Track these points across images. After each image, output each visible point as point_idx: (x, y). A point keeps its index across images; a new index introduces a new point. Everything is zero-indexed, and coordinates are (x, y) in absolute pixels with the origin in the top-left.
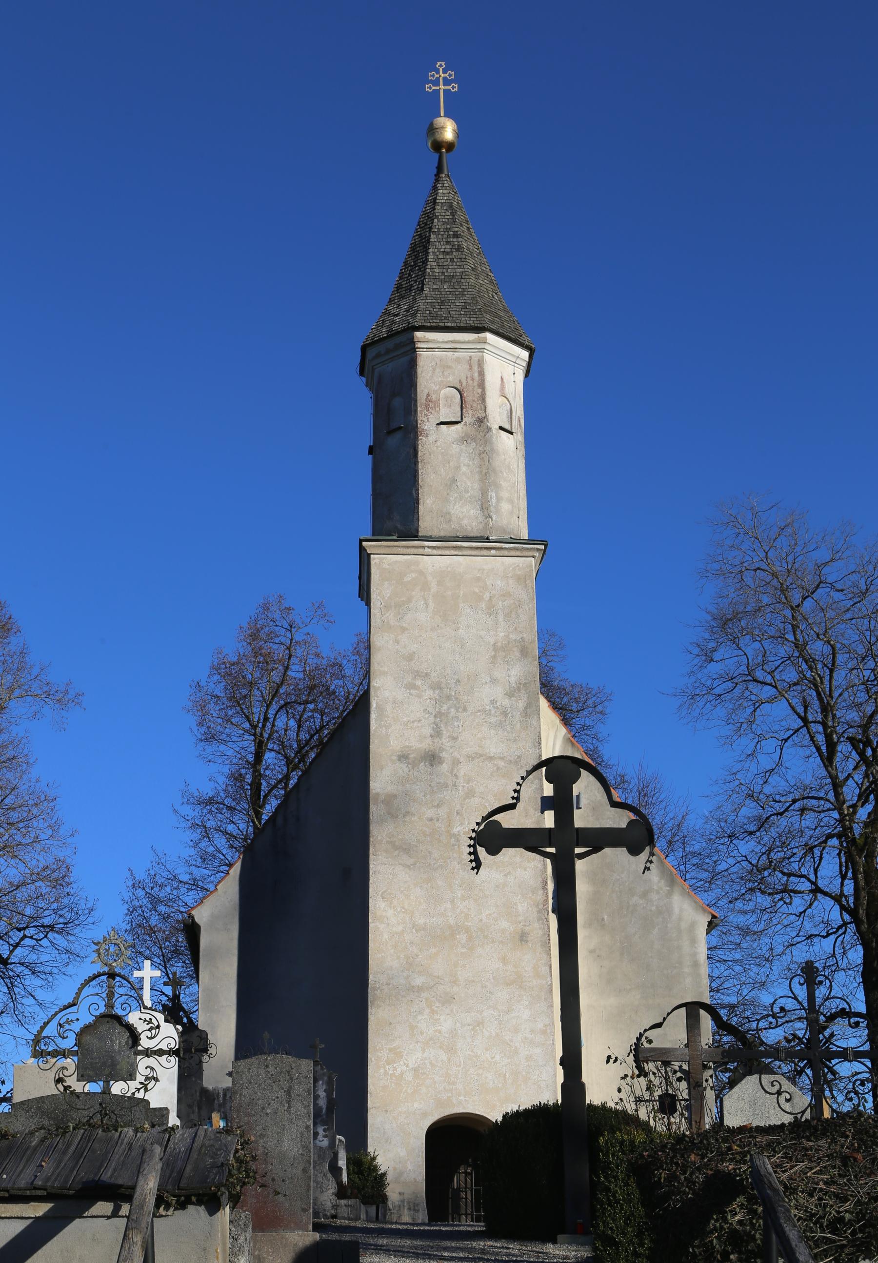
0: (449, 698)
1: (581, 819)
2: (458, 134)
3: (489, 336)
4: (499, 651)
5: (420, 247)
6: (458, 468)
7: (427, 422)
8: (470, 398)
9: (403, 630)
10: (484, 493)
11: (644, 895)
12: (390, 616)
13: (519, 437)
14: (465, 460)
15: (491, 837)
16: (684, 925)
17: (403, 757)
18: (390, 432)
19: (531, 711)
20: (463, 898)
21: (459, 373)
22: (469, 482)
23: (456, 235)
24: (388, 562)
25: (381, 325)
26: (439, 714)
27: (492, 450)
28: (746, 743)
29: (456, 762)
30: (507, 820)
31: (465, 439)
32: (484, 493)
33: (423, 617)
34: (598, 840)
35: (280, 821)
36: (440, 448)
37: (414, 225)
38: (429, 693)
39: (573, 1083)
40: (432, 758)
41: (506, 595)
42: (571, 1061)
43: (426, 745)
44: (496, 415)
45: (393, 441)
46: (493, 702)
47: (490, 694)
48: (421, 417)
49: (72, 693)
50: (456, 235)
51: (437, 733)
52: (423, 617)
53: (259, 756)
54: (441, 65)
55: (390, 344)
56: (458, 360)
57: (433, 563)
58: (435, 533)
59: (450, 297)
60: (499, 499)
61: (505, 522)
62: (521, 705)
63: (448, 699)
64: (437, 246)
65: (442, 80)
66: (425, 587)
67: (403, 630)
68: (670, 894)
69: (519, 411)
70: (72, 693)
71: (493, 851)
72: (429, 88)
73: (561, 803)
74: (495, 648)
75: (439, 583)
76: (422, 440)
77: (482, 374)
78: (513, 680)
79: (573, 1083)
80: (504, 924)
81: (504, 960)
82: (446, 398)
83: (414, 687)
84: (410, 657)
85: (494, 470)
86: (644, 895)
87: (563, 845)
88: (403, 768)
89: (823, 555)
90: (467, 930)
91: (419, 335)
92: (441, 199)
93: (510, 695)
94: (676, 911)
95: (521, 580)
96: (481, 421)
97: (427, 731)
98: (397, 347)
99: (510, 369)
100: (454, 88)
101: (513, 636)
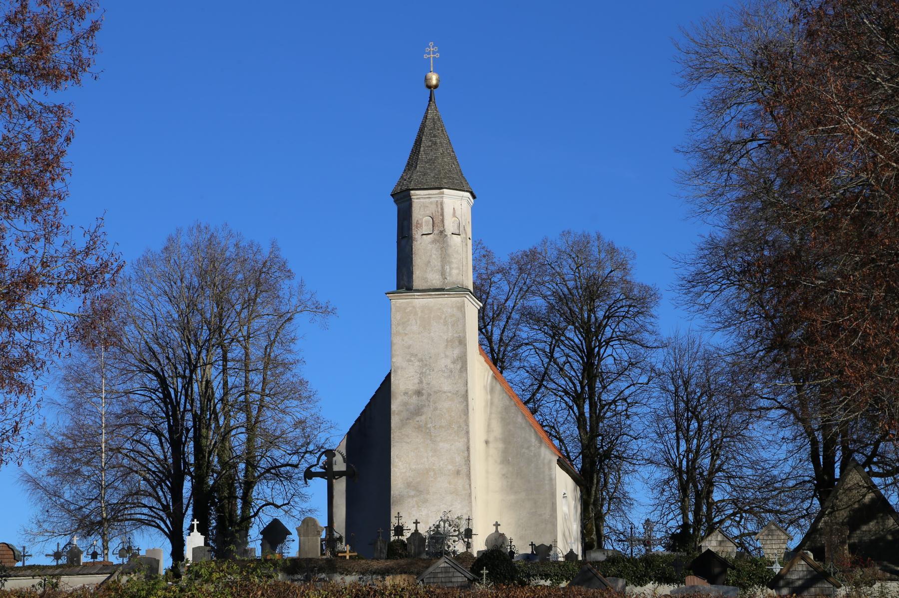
0: (426, 365)
2: (438, 80)
3: (445, 190)
6: (431, 256)
7: (417, 234)
8: (438, 221)
9: (406, 334)
10: (443, 267)
11: (528, 448)
12: (400, 328)
16: (546, 461)
17: (406, 393)
20: (432, 456)
21: (432, 209)
22: (436, 262)
24: (401, 302)
25: (398, 185)
26: (422, 373)
27: (448, 245)
29: (429, 395)
30: (313, 470)
31: (434, 241)
32: (443, 267)
33: (415, 328)
35: (362, 419)
36: (423, 246)
38: (417, 363)
40: (419, 393)
43: (416, 387)
44: (450, 225)
45: (403, 242)
46: (446, 366)
48: (414, 232)
50: (435, 136)
51: (421, 382)
54: (431, 44)
56: (431, 203)
57: (418, 302)
58: (420, 288)
59: (428, 171)
60: (451, 269)
61: (454, 279)
62: (459, 367)
63: (425, 365)
64: (425, 142)
65: (432, 52)
66: (416, 314)
67: (406, 334)
68: (540, 447)
72: (426, 56)
74: (447, 341)
75: (422, 312)
77: (442, 209)
78: (455, 356)
80: (450, 467)
81: (450, 483)
82: (426, 222)
83: (411, 361)
84: (409, 347)
85: (449, 255)
86: (528, 448)
88: (406, 398)
90: (434, 470)
91: (412, 192)
93: (454, 363)
94: (543, 455)
96: (441, 232)
97: (416, 381)
100: (437, 55)
101: (455, 335)
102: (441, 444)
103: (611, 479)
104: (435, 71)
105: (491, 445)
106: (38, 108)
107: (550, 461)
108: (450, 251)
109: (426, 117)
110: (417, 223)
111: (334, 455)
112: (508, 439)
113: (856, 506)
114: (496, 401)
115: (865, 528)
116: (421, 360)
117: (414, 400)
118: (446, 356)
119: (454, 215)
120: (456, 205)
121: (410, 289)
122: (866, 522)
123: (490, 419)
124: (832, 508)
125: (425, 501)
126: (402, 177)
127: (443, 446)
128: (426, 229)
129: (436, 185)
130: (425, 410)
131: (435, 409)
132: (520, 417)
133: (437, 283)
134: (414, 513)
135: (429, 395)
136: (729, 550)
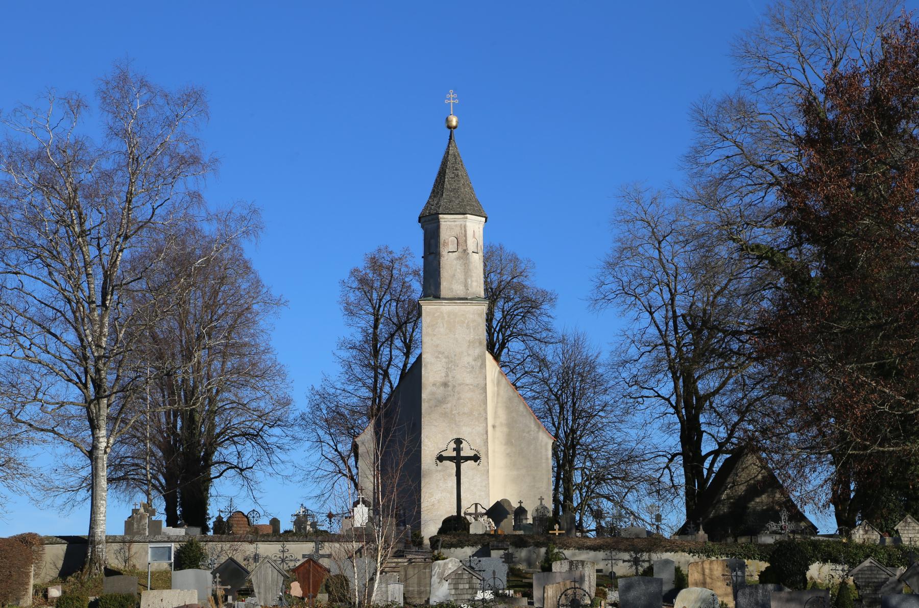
1: (463, 454)
2: (457, 122)
4: (471, 343)
5: (442, 174)
7: (444, 251)
8: (461, 241)
10: (466, 280)
12: (430, 330)
13: (481, 254)
14: (458, 267)
15: (476, 458)
17: (434, 385)
18: (430, 254)
19: (483, 365)
21: (457, 231)
22: (460, 276)
23: (457, 169)
24: (429, 308)
25: (426, 208)
29: (454, 386)
30: (445, 454)
31: (458, 258)
32: (466, 280)
34: (467, 459)
36: (449, 261)
37: (440, 163)
38: (444, 360)
40: (445, 385)
41: (474, 321)
43: (443, 380)
44: (471, 246)
45: (431, 257)
47: (467, 360)
48: (441, 249)
49: (283, 301)
50: (457, 169)
51: (447, 376)
52: (442, 330)
53: (376, 327)
55: (430, 218)
56: (456, 226)
57: (445, 308)
58: (447, 297)
60: (472, 281)
62: (479, 364)
63: (451, 362)
64: (449, 174)
65: (452, 99)
68: (538, 432)
69: (481, 243)
70: (283, 301)
71: (441, 461)
72: (446, 102)
73: (458, 450)
75: (449, 317)
76: (442, 259)
77: (465, 231)
84: (437, 346)
87: (458, 460)
88: (434, 389)
91: (441, 216)
92: (451, 152)
95: (480, 315)
96: (465, 251)
97: (443, 375)
98: (433, 219)
99: (477, 226)
100: (457, 101)
102: (464, 428)
104: (454, 114)
105: (497, 429)
107: (546, 444)
108: (471, 267)
109: (447, 153)
110: (444, 242)
111: (461, 443)
112: (511, 424)
113: (752, 482)
114: (502, 392)
115: (758, 500)
116: (447, 357)
117: (440, 391)
118: (469, 355)
119: (474, 237)
120: (474, 225)
121: (437, 297)
122: (759, 495)
123: (496, 407)
124: (733, 483)
126: (428, 202)
128: (452, 247)
129: (461, 211)
130: (450, 399)
131: (459, 399)
134: (441, 485)
135: (454, 386)
136: (874, 537)
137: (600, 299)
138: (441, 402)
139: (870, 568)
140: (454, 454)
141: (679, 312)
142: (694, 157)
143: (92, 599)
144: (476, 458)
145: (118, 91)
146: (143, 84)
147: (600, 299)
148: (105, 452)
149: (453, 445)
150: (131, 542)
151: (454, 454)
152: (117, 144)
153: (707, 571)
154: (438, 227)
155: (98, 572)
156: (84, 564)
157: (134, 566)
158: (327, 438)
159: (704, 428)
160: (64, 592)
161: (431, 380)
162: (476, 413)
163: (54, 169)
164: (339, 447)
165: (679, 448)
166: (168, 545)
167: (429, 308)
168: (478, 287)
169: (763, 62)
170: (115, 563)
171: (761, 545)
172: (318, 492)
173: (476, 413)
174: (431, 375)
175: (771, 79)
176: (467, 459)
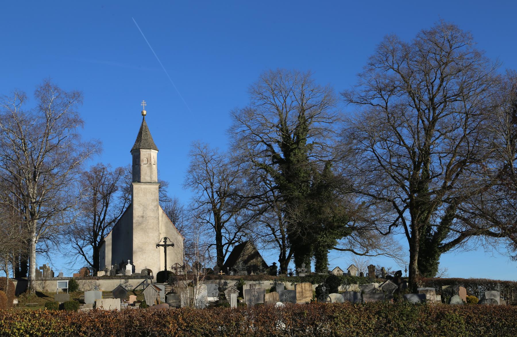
1: (167, 243)
4: (153, 200)
5: (140, 133)
7: (142, 164)
8: (149, 160)
12: (136, 195)
15: (158, 245)
17: (138, 217)
19: (158, 209)
21: (147, 156)
22: (148, 173)
24: (136, 186)
25: (134, 146)
28: (196, 191)
31: (148, 167)
34: (169, 245)
36: (144, 168)
39: (166, 269)
40: (143, 217)
42: (166, 267)
44: (153, 162)
45: (136, 166)
57: (143, 186)
63: (145, 208)
64: (143, 133)
65: (144, 104)
69: (156, 161)
73: (165, 242)
79: (166, 269)
87: (165, 246)
88: (138, 218)
89: (213, 154)
103: (252, 253)
106: (363, 94)
109: (142, 125)
116: (143, 206)
117: (140, 219)
120: (154, 153)
121: (139, 182)
122: (252, 259)
125: (145, 253)
127: (151, 235)
128: (145, 162)
132: (171, 225)
133: (149, 180)
137: (186, 185)
138: (140, 224)
139: (388, 284)
140: (164, 243)
141: (214, 190)
142: (231, 130)
143: (60, 303)
144: (173, 245)
145: (44, 91)
146: (56, 89)
147: (186, 185)
148: (35, 242)
149: (163, 240)
150: (46, 280)
151: (164, 243)
152: (42, 114)
153: (303, 287)
154: (140, 154)
155: (33, 293)
156: (26, 289)
157: (47, 290)
158: (73, 239)
159: (222, 234)
160: (19, 302)
161: (137, 215)
162: (155, 228)
163: (14, 122)
164: (79, 244)
165: (215, 243)
166: (66, 281)
167: (136, 186)
168: (155, 178)
169: (261, 96)
170: (39, 289)
171: (301, 277)
172: (69, 261)
173: (155, 228)
174: (137, 212)
175: (261, 102)
176: (169, 245)
